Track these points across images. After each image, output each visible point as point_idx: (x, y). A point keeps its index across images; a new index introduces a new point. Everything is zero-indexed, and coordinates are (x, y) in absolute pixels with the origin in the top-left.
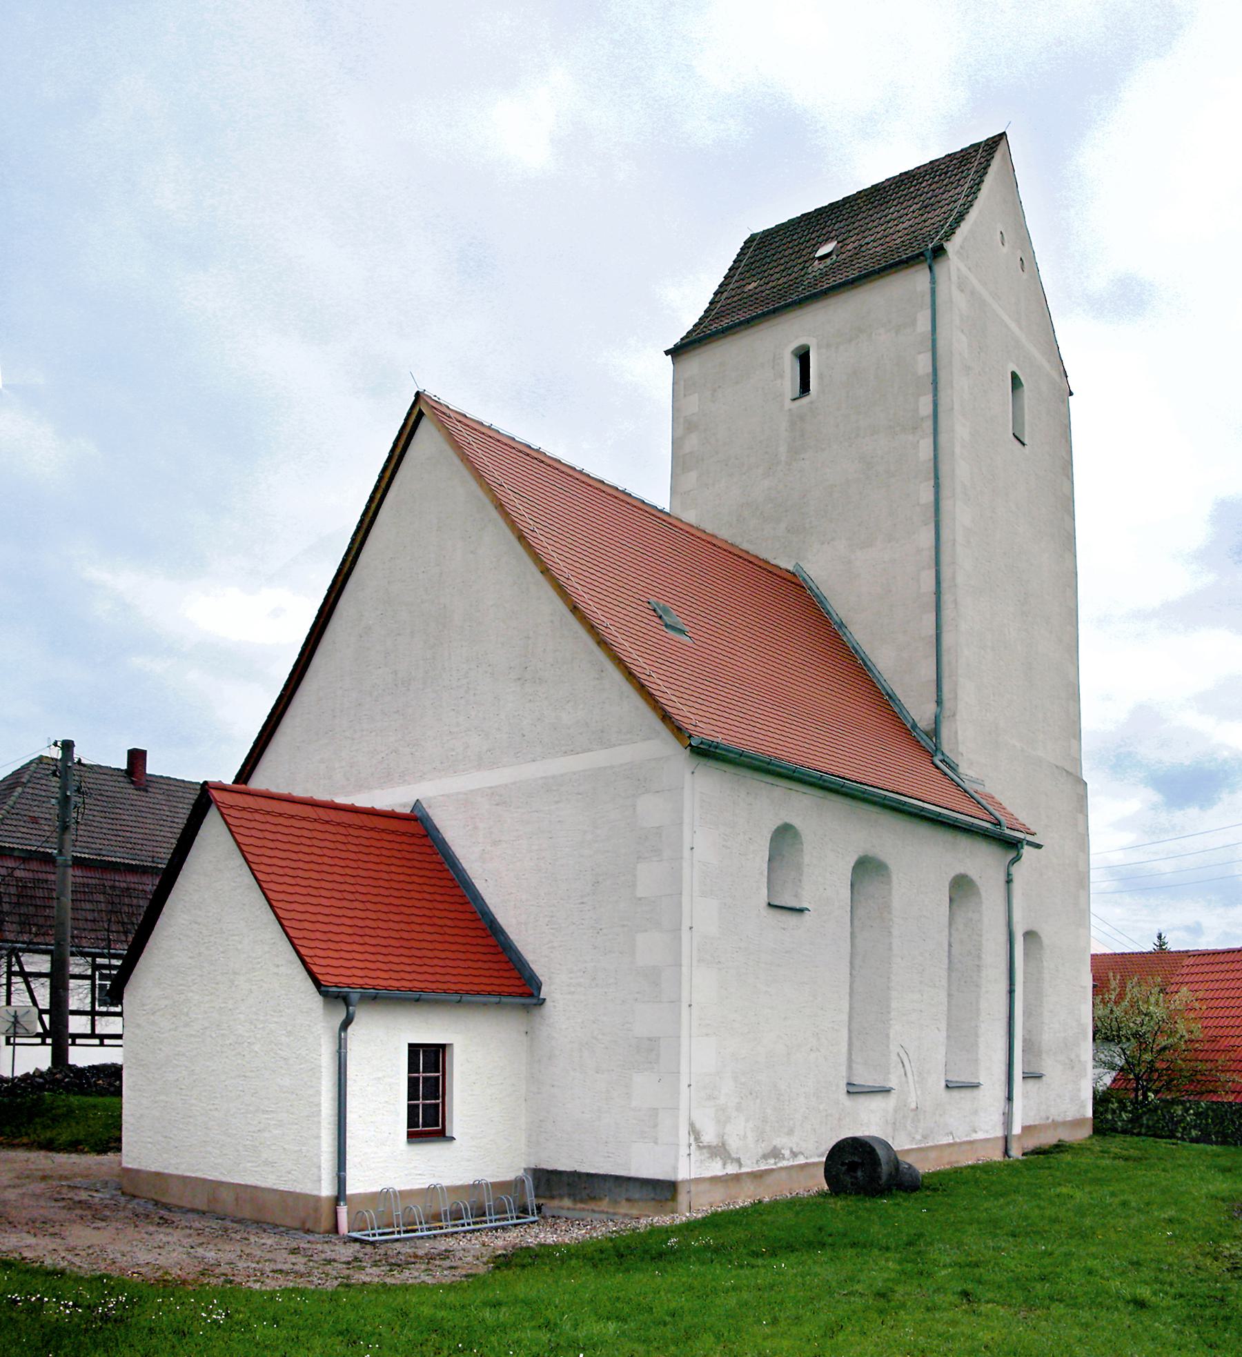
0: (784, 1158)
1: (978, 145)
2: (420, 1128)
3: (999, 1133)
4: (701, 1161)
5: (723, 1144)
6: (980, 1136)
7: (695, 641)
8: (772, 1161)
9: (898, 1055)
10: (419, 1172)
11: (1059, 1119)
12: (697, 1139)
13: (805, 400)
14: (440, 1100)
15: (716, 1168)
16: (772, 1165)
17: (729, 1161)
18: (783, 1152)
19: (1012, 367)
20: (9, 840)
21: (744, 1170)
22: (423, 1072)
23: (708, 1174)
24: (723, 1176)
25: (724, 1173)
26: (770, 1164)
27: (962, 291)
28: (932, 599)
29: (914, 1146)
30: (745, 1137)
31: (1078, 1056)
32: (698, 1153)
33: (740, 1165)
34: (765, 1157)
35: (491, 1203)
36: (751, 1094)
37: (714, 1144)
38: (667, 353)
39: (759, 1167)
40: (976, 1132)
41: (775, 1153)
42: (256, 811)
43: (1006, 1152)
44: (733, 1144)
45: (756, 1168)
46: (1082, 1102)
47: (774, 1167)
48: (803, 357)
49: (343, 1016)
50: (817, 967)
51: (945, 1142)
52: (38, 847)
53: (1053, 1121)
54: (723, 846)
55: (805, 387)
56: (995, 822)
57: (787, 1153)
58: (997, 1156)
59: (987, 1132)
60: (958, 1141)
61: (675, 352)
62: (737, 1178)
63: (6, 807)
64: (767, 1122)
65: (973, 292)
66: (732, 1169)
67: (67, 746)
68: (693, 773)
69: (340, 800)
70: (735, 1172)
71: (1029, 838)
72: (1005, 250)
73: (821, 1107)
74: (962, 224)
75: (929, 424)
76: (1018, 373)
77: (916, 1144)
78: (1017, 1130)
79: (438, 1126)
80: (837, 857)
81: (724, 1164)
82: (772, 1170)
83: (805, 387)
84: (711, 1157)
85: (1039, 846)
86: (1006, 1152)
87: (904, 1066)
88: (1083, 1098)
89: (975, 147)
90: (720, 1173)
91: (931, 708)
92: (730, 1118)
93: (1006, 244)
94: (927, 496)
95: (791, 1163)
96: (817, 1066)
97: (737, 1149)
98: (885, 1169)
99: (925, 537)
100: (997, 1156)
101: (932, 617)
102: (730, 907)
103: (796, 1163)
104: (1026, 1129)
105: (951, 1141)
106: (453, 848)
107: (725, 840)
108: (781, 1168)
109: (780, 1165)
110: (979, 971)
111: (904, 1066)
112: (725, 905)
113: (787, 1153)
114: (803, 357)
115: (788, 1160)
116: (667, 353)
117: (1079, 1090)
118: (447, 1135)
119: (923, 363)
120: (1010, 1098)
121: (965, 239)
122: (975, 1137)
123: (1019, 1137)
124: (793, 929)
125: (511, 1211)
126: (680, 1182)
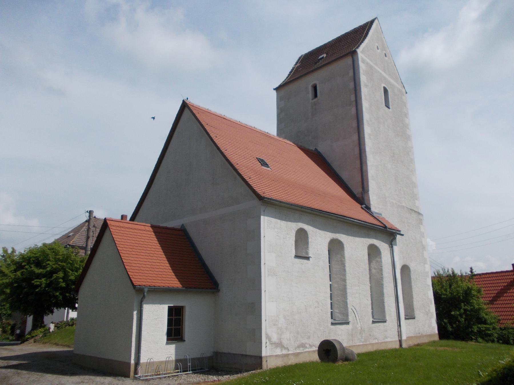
0: (306, 348)
1: (369, 22)
2: (173, 337)
3: (397, 339)
4: (272, 349)
5: (281, 342)
6: (389, 340)
7: (272, 169)
8: (301, 349)
9: (352, 309)
10: (171, 354)
11: (424, 334)
12: (270, 340)
13: (316, 99)
14: (181, 327)
15: (278, 352)
16: (302, 350)
17: (284, 349)
18: (306, 345)
19: (383, 85)
20: (78, 243)
21: (290, 352)
22: (175, 316)
23: (275, 354)
24: (281, 355)
25: (282, 353)
26: (301, 350)
27: (363, 63)
28: (358, 156)
29: (361, 344)
30: (290, 339)
31: (429, 310)
32: (270, 345)
33: (288, 350)
34: (298, 347)
35: (190, 364)
36: (291, 323)
37: (277, 342)
38: (274, 89)
39: (296, 351)
40: (387, 338)
41: (303, 346)
42: (123, 227)
43: (401, 345)
44: (285, 342)
45: (295, 352)
46: (433, 327)
47: (302, 351)
48: (315, 88)
49: (142, 296)
50: (316, 277)
51: (375, 342)
52: (83, 245)
53: (422, 334)
54: (277, 236)
55: (316, 95)
56: (384, 226)
57: (308, 346)
58: (397, 346)
59: (392, 338)
60: (380, 341)
61: (277, 89)
62: (288, 355)
63: (79, 233)
64: (299, 334)
65: (367, 63)
66: (285, 352)
67: (91, 213)
68: (264, 211)
69: (161, 225)
70: (286, 353)
71: (398, 232)
72: (379, 51)
73: (321, 328)
74: (362, 44)
75: (354, 103)
76: (386, 87)
77: (362, 343)
78: (404, 337)
79: (180, 336)
80: (322, 239)
81: (282, 350)
82: (302, 353)
83: (316, 95)
84: (276, 347)
85: (403, 235)
86: (401, 345)
87: (354, 313)
88: (433, 326)
89: (367, 23)
90: (280, 354)
91: (360, 190)
92: (283, 332)
93: (376, 47)
94: (355, 124)
95: (310, 350)
96: (318, 313)
97: (287, 344)
98: (339, 353)
99: (355, 137)
100: (397, 346)
101: (358, 162)
102: (280, 256)
103: (312, 350)
104: (409, 338)
105: (377, 342)
106: (193, 240)
107: (277, 234)
108: (306, 352)
109: (305, 350)
110: (382, 279)
111: (354, 313)
112: (278, 255)
113: (308, 346)
114: (315, 88)
115: (308, 348)
116: (274, 89)
117: (431, 323)
118: (183, 339)
119: (352, 85)
120: (400, 326)
121: (364, 48)
122: (387, 340)
123: (406, 340)
124: (306, 264)
125: (180, 369)
126: (263, 357)
